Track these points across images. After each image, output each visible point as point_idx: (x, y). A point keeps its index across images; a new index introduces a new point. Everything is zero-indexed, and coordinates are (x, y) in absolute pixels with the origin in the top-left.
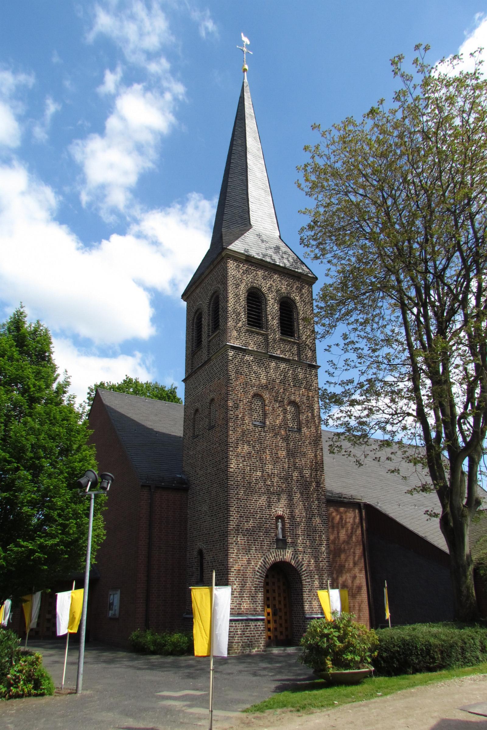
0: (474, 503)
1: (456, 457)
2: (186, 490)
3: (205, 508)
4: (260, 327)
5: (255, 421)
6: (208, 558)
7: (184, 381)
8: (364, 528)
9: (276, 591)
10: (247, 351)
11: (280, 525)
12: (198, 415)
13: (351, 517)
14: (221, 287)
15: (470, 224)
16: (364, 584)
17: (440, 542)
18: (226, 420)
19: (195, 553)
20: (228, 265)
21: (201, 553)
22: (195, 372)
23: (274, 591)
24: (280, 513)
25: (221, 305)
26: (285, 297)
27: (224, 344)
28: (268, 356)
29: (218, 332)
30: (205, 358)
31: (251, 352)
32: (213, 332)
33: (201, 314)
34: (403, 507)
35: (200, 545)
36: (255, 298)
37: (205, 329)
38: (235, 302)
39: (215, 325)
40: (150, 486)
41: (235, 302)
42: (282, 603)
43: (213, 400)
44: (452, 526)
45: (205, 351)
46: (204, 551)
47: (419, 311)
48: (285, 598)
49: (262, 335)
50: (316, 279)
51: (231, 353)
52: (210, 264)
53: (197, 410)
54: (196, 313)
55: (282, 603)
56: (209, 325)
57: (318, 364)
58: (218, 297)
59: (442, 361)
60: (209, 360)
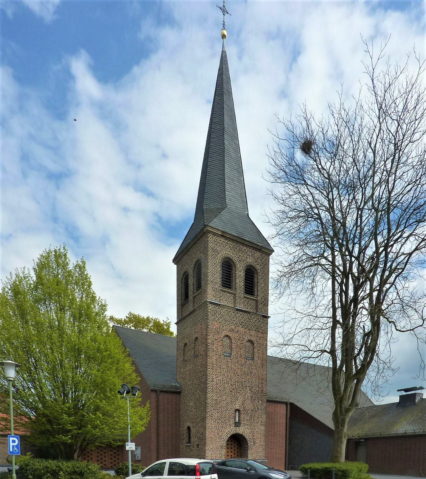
0: (355, 405)
1: (349, 377)
2: (179, 393)
3: (192, 404)
4: (230, 287)
5: (225, 353)
6: (193, 431)
7: (176, 323)
8: (288, 417)
9: (233, 452)
10: (221, 305)
11: (237, 414)
12: (186, 347)
13: (282, 410)
14: (203, 256)
15: (420, 241)
16: (271, 286)
17: (331, 424)
18: (206, 352)
19: (186, 428)
20: (209, 239)
21: (189, 428)
22: (184, 318)
23: (232, 452)
24: (238, 408)
25: (203, 271)
26: (249, 265)
27: (205, 300)
28: (235, 309)
29: (201, 290)
30: (191, 308)
31: (224, 306)
32: (197, 290)
33: (188, 275)
34: (313, 405)
35: (188, 424)
36: (228, 266)
37: (191, 288)
38: (213, 273)
39: (198, 285)
40: (156, 391)
41: (213, 273)
42: (236, 454)
43: (196, 338)
44: (338, 417)
45: (191, 304)
46: (191, 427)
47: (342, 281)
48: (238, 452)
49: (232, 294)
50: (273, 251)
51: (210, 307)
52: (195, 238)
53: (186, 344)
54: (184, 274)
55: (236, 454)
56: (194, 285)
57: (269, 315)
58: (200, 264)
59: (352, 316)
60: (194, 311)
